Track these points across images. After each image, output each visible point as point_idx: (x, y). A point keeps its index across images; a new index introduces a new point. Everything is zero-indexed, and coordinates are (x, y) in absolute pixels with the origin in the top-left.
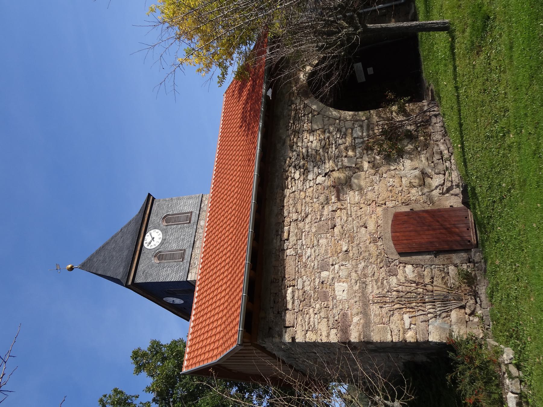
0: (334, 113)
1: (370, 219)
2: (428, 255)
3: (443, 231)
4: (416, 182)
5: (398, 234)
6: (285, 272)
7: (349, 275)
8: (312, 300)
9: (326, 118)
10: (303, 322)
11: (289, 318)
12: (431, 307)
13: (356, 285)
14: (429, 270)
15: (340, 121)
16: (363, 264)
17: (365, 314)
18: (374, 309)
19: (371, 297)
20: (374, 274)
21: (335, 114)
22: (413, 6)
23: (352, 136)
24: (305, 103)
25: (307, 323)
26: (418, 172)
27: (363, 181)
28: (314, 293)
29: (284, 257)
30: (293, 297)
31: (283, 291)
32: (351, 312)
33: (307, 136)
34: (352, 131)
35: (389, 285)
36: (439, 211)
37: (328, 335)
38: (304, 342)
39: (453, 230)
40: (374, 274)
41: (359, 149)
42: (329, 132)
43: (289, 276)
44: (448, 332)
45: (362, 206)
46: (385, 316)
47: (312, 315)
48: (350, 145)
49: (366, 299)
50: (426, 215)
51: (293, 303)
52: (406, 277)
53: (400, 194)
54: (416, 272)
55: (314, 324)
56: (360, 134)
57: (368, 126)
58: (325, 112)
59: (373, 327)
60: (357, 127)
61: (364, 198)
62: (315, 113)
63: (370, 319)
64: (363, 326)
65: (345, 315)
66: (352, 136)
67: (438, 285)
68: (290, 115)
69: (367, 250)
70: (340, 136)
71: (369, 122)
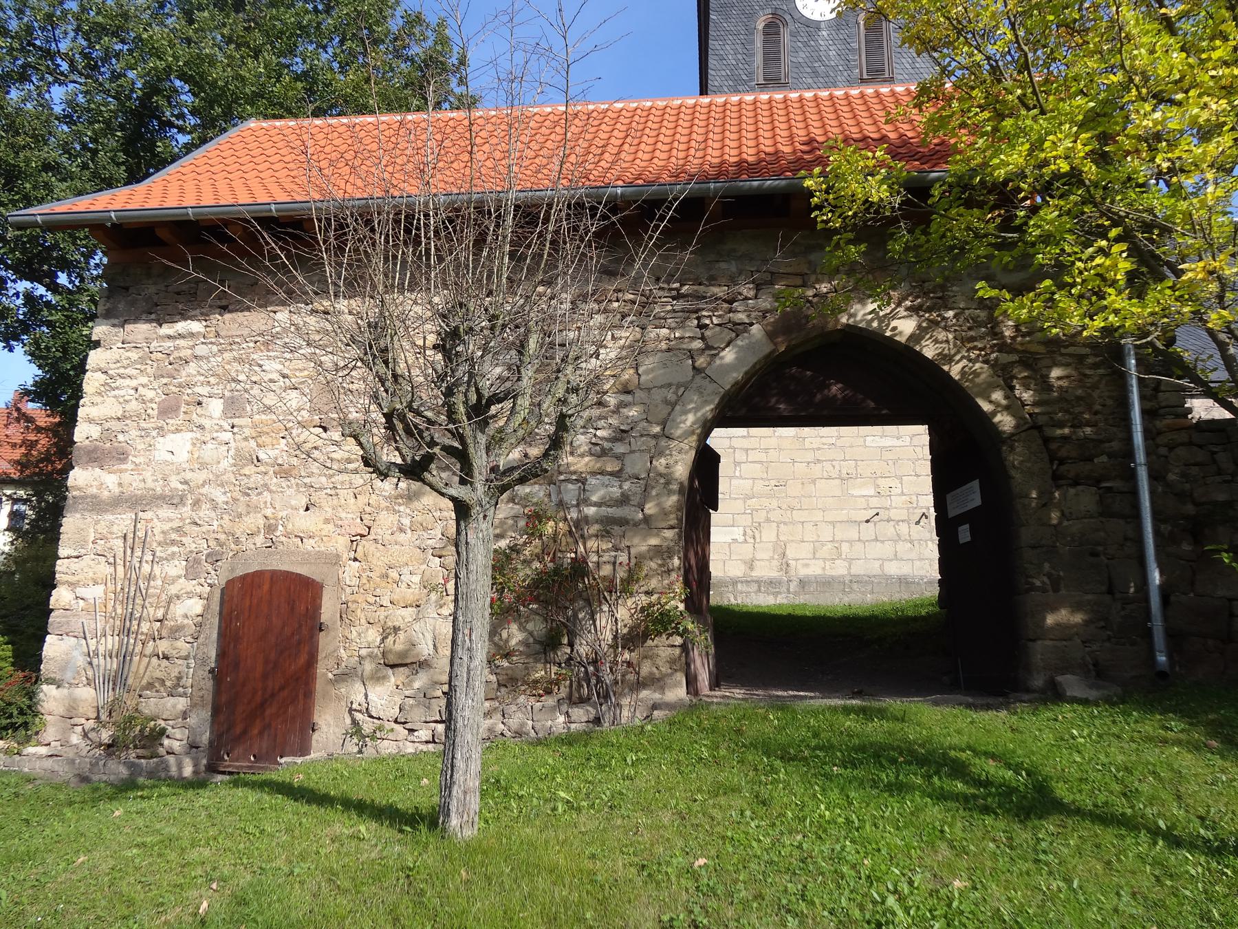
0: (691, 418)
1: (322, 519)
2: (217, 655)
3: (258, 699)
4: (397, 644)
5: (266, 587)
6: (237, 311)
7: (203, 466)
8: (165, 381)
9: (676, 393)
10: (125, 362)
11: (141, 330)
12: (110, 647)
13: (181, 483)
14: (184, 653)
15: (655, 436)
16: (221, 499)
17: (117, 502)
18: (122, 521)
19: (149, 515)
20: (196, 524)
21: (684, 422)
22: (1093, 694)
23: (593, 474)
24: (751, 324)
25: (122, 371)
26: (426, 652)
27: (431, 503)
28: (180, 386)
29: (271, 304)
30: (181, 336)
31: (198, 312)
32: (126, 470)
33: (620, 338)
34: (611, 474)
35: (166, 559)
36: (309, 694)
37: (90, 421)
38: (87, 367)
39: (258, 721)
40: (196, 524)
41: (542, 494)
42: (622, 405)
43: (227, 322)
44: (58, 677)
45: (362, 499)
46: (108, 545)
47: (134, 383)
48: (562, 469)
49: (147, 504)
50: (303, 659)
51: (169, 337)
52: (178, 597)
53: (372, 599)
54: (186, 621)
55: (117, 388)
56: (594, 498)
57: (623, 522)
58: (700, 391)
59: (90, 518)
60: (621, 487)
61: (384, 504)
62: (701, 361)
63: (107, 511)
64: (94, 497)
65: (122, 456)
66: (593, 474)
67: (150, 668)
68: (712, 280)
69: (252, 509)
70: (602, 439)
71: (636, 524)
